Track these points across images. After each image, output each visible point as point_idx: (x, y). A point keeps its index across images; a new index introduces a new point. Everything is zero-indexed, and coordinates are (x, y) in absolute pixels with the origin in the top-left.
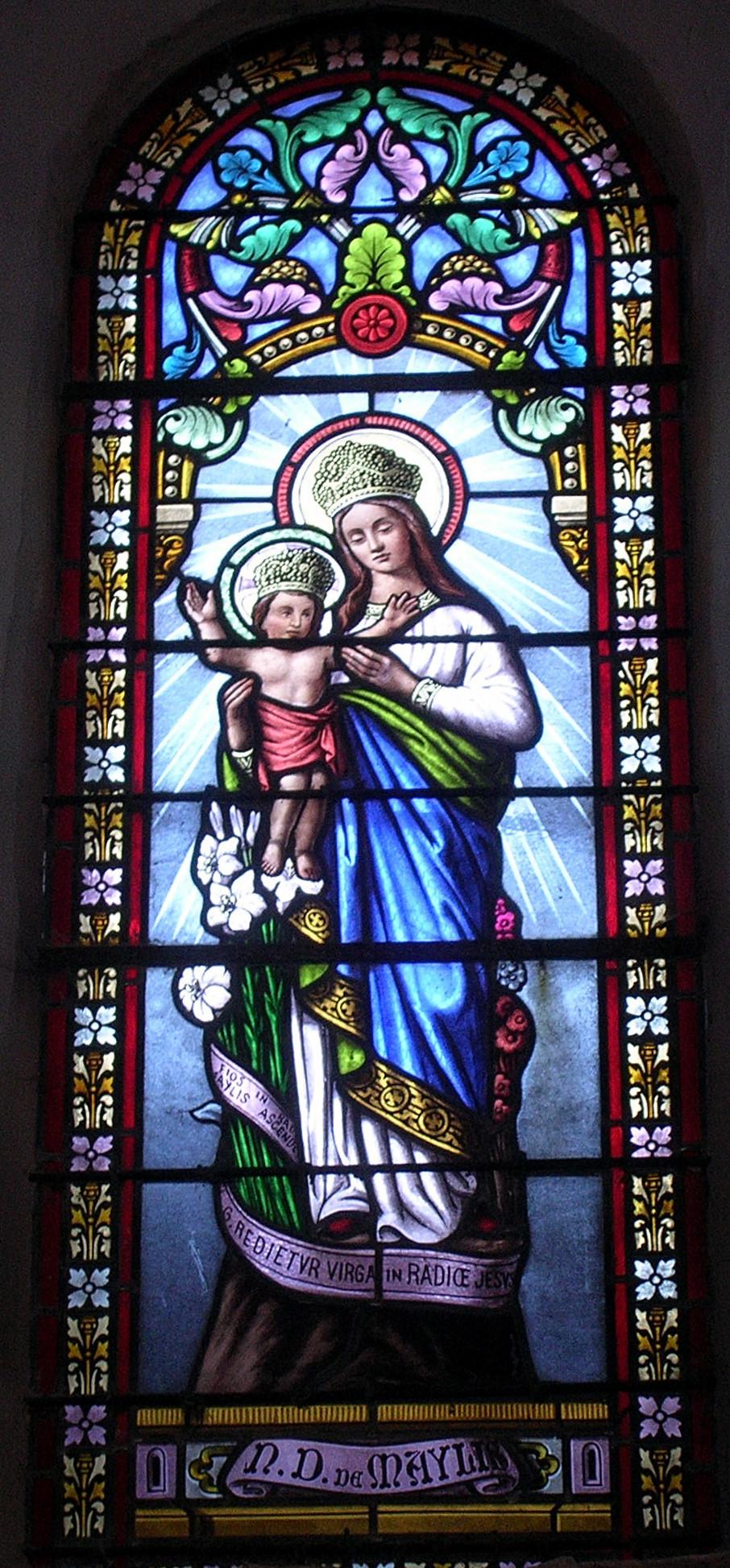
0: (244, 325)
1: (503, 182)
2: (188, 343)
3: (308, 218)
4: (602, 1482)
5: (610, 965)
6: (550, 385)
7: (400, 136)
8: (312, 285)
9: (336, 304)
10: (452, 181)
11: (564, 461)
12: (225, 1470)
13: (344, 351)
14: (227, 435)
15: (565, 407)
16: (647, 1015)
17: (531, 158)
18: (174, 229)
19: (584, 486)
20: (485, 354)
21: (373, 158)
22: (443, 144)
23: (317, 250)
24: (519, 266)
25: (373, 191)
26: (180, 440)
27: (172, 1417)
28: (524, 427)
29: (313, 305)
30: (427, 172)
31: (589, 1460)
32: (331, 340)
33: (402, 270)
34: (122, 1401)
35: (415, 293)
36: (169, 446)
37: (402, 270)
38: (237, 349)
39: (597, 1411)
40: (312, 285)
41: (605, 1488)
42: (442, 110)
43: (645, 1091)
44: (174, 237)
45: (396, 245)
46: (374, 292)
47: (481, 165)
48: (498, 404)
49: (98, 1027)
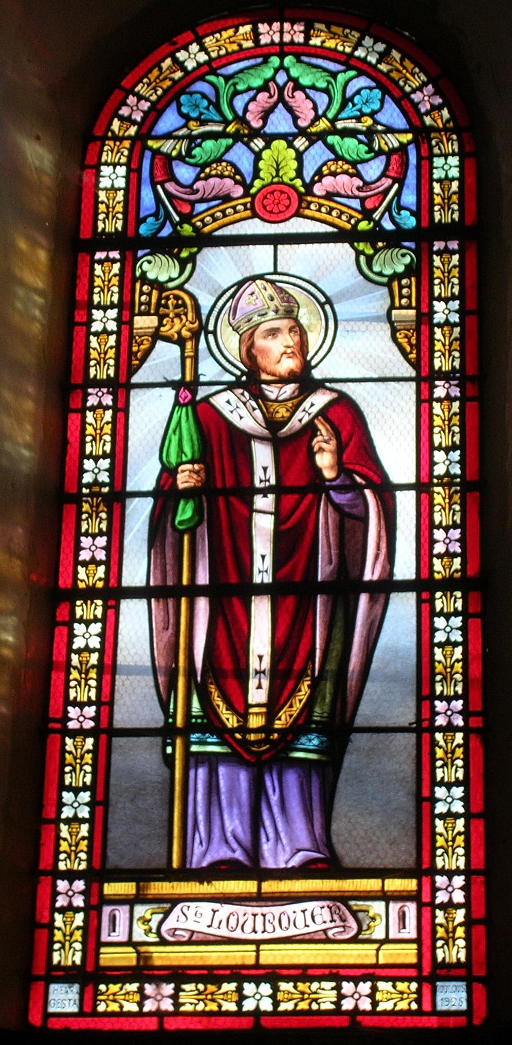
0: (192, 203)
1: (363, 115)
2: (156, 215)
3: (237, 137)
4: (411, 931)
5: (425, 595)
6: (395, 239)
7: (298, 86)
8: (238, 177)
9: (253, 191)
10: (330, 115)
11: (401, 287)
12: (161, 923)
13: (257, 220)
14: (181, 273)
15: (403, 255)
16: (447, 629)
17: (382, 101)
18: (150, 143)
19: (414, 304)
20: (349, 222)
21: (281, 99)
22: (326, 91)
23: (241, 156)
24: (373, 170)
25: (280, 122)
26: (151, 276)
27: (127, 888)
28: (376, 269)
29: (240, 191)
30: (315, 108)
31: (402, 917)
32: (248, 213)
33: (296, 170)
34: (96, 875)
35: (304, 185)
36: (144, 278)
37: (296, 170)
38: (186, 218)
39: (411, 885)
40: (238, 177)
41: (413, 935)
42: (325, 70)
43: (443, 208)
44: (150, 149)
45: (292, 153)
46: (278, 183)
47: (350, 105)
48: (358, 253)
49: (86, 636)
